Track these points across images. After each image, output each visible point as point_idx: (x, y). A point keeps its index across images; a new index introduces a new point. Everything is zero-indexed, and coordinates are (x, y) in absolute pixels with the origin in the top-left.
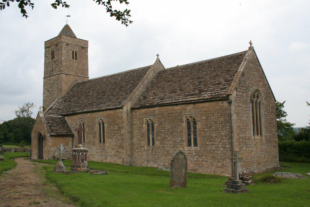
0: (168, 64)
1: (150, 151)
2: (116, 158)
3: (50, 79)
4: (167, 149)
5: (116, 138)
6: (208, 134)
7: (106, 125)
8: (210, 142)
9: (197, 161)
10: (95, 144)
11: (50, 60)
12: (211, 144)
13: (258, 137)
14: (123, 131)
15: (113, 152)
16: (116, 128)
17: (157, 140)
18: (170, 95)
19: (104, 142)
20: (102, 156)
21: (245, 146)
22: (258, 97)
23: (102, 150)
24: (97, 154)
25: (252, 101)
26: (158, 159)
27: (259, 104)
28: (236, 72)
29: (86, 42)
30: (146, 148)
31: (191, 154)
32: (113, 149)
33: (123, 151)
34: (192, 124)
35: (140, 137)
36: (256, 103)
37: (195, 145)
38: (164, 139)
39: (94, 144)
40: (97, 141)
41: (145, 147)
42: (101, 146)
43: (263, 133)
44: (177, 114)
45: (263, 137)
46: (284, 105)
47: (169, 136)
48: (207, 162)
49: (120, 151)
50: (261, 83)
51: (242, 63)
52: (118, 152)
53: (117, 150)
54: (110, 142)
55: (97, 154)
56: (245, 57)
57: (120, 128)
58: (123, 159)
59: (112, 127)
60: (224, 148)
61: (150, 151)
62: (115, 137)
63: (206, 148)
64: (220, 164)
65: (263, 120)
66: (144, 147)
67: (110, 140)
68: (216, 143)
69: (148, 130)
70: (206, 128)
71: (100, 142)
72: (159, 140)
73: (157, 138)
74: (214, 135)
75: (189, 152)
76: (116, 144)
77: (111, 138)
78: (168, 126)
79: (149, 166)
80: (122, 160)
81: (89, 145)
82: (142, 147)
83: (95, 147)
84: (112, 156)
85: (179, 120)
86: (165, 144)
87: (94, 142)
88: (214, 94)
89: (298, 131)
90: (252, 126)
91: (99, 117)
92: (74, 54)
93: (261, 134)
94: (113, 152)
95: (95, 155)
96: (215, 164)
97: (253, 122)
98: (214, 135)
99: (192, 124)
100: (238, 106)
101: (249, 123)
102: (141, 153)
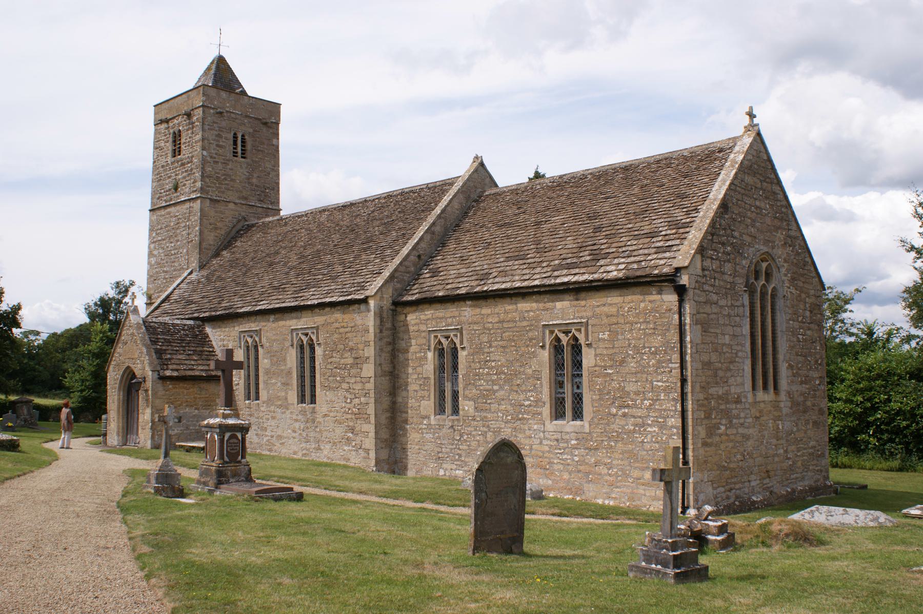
2: (346, 448)
3: (169, 213)
4: (494, 425)
5: (347, 391)
6: (615, 384)
9: (582, 462)
15: (339, 431)
16: (350, 361)
19: (313, 401)
22: (768, 276)
28: (704, 199)
29: (274, 108)
30: (433, 422)
34: (567, 356)
35: (417, 388)
36: (763, 294)
37: (578, 414)
39: (285, 406)
40: (293, 396)
41: (432, 417)
42: (303, 412)
43: (783, 383)
44: (525, 323)
45: (783, 396)
47: (501, 388)
50: (780, 236)
52: (352, 430)
53: (351, 424)
55: (294, 435)
56: (732, 156)
62: (345, 386)
66: (428, 417)
70: (611, 367)
71: (302, 400)
73: (467, 392)
75: (558, 436)
76: (348, 406)
78: (498, 358)
84: (334, 443)
85: (531, 340)
93: (776, 388)
94: (339, 431)
96: (636, 473)
98: (631, 387)
101: (740, 354)
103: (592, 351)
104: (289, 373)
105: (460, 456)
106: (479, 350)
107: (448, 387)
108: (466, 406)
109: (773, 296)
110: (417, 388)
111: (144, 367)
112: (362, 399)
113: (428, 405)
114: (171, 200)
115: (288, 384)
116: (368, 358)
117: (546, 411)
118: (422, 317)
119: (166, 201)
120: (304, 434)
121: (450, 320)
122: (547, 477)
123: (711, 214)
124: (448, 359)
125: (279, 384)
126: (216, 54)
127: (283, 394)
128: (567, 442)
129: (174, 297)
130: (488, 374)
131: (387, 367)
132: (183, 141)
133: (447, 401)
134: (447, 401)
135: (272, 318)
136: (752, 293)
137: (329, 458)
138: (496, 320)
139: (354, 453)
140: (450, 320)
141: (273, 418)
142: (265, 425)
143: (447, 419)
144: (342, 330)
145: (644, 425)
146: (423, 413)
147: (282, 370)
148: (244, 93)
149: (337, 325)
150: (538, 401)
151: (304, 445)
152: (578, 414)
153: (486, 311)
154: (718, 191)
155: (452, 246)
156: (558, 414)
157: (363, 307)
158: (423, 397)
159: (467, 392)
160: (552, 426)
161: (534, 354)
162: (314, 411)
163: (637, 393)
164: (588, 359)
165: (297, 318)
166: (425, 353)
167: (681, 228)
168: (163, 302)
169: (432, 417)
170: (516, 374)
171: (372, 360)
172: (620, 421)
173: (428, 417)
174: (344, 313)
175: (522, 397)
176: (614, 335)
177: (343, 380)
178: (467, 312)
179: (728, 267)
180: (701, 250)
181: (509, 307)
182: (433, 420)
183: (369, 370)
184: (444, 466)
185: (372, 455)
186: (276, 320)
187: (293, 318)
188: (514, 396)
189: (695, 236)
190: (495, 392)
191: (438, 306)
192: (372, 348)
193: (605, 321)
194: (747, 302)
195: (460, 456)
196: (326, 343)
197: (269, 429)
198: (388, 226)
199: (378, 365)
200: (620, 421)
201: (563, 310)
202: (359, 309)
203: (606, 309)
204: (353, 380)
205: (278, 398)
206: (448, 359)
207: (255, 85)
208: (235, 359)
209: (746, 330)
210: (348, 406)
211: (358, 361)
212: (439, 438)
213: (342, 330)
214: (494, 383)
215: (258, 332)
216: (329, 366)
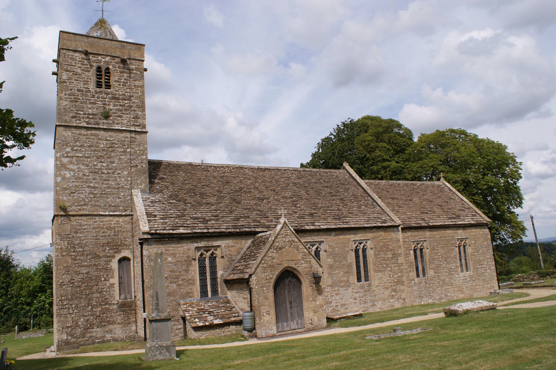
0: (356, 119)
1: (423, 284)
2: (391, 301)
3: (96, 135)
4: (442, 278)
5: (390, 271)
6: (477, 258)
7: (370, 253)
8: (480, 265)
9: (472, 286)
10: (350, 284)
12: (481, 268)
14: (401, 260)
16: (391, 256)
19: (367, 279)
20: (365, 302)
23: (366, 293)
24: (355, 301)
26: (433, 292)
30: (416, 281)
31: (466, 279)
32: (387, 288)
33: (402, 288)
35: (407, 267)
38: (439, 266)
39: (348, 285)
40: (353, 278)
42: (362, 287)
44: (449, 238)
46: (11, 43)
47: (443, 263)
48: (479, 285)
49: (398, 289)
52: (395, 291)
53: (394, 288)
55: (355, 301)
57: (395, 256)
58: (404, 299)
59: (382, 255)
60: (490, 270)
61: (423, 284)
62: (389, 269)
64: (489, 286)
66: (414, 280)
67: (380, 275)
68: (484, 266)
69: (416, 257)
71: (359, 280)
72: (432, 269)
73: (431, 266)
74: (482, 258)
75: (464, 278)
76: (392, 279)
77: (382, 271)
78: (441, 251)
79: (423, 303)
80: (401, 301)
81: (337, 288)
82: (412, 280)
83: (350, 290)
84: (384, 300)
85: (452, 244)
86: (440, 273)
87: (348, 281)
89: (333, 234)
94: (387, 293)
95: (351, 304)
96: (486, 286)
98: (482, 258)
102: (410, 289)
103: (470, 247)
105: (430, 293)
106: (433, 249)
107: (420, 265)
108: (430, 273)
110: (407, 267)
112: (399, 274)
114: (98, 124)
115: (349, 272)
116: (400, 254)
118: (406, 235)
119: (88, 123)
120: (363, 299)
121: (420, 237)
122: (462, 294)
125: (342, 273)
126: (100, 16)
127: (346, 278)
128: (466, 279)
130: (438, 258)
135: (333, 233)
137: (380, 309)
138: (439, 237)
139: (396, 302)
140: (420, 237)
141: (337, 294)
142: (330, 300)
144: (384, 241)
145: (486, 270)
146: (411, 278)
147: (344, 265)
149: (381, 238)
150: (456, 266)
151: (363, 305)
153: (435, 233)
156: (462, 271)
157: (395, 229)
158: (410, 271)
159: (431, 266)
160: (461, 274)
161: (454, 249)
162: (370, 285)
165: (354, 234)
166: (409, 251)
170: (448, 257)
172: (480, 270)
173: (414, 280)
174: (385, 232)
175: (451, 265)
176: (475, 241)
178: (428, 233)
181: (444, 232)
182: (416, 280)
184: (423, 300)
186: (337, 235)
187: (352, 234)
188: (448, 266)
190: (441, 265)
191: (414, 230)
193: (473, 237)
195: (430, 293)
196: (375, 248)
197: (334, 301)
200: (480, 270)
201: (461, 233)
203: (472, 233)
204: (393, 265)
205: (341, 282)
210: (392, 279)
212: (420, 288)
213: (384, 241)
214: (441, 261)
215: (321, 242)
216: (378, 260)
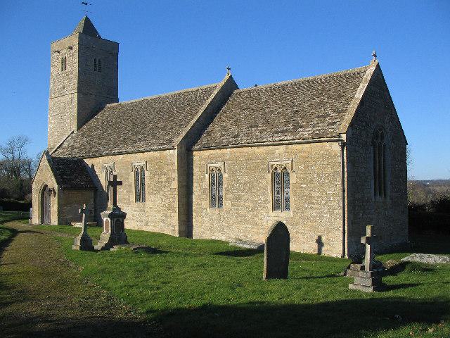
3: (60, 101)
8: (309, 204)
11: (60, 72)
13: (380, 199)
15: (159, 216)
17: (227, 199)
18: (305, 264)
21: (362, 211)
22: (382, 138)
25: (374, 144)
27: (384, 148)
28: (352, 98)
29: (115, 46)
34: (280, 179)
36: (380, 147)
37: (287, 208)
41: (208, 209)
43: (388, 192)
45: (388, 199)
50: (388, 117)
51: (361, 85)
54: (151, 200)
56: (365, 76)
63: (303, 213)
65: (388, 174)
67: (153, 198)
70: (304, 184)
73: (228, 196)
88: (318, 132)
90: (373, 181)
91: (138, 159)
92: (97, 63)
93: (385, 195)
97: (375, 175)
99: (280, 179)
100: (355, 151)
101: (369, 177)
104: (130, 186)
108: (227, 204)
109: (384, 148)
111: (53, 183)
113: (206, 203)
117: (270, 206)
123: (356, 106)
124: (216, 181)
129: (66, 144)
131: (185, 184)
132: (67, 63)
133: (216, 201)
134: (216, 201)
136: (374, 146)
143: (216, 211)
148: (99, 36)
152: (287, 208)
154: (359, 95)
155: (216, 120)
163: (319, 197)
164: (293, 179)
167: (340, 112)
168: (58, 148)
169: (208, 209)
171: (176, 178)
177: (161, 189)
179: (364, 133)
180: (352, 125)
183: (175, 184)
185: (177, 228)
189: (349, 117)
192: (176, 182)
194: (372, 151)
198: (180, 110)
199: (179, 182)
202: (170, 208)
206: (216, 181)
207: (105, 33)
208: (118, 186)
209: (372, 165)
211: (169, 180)
